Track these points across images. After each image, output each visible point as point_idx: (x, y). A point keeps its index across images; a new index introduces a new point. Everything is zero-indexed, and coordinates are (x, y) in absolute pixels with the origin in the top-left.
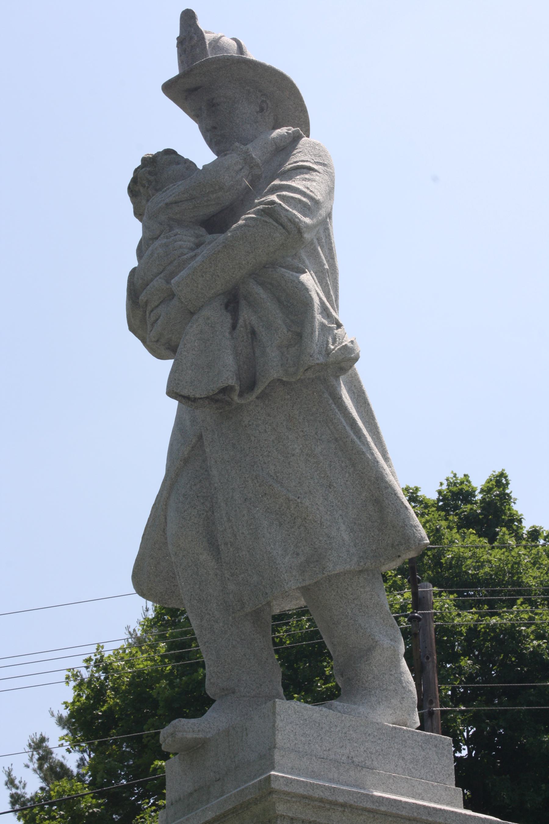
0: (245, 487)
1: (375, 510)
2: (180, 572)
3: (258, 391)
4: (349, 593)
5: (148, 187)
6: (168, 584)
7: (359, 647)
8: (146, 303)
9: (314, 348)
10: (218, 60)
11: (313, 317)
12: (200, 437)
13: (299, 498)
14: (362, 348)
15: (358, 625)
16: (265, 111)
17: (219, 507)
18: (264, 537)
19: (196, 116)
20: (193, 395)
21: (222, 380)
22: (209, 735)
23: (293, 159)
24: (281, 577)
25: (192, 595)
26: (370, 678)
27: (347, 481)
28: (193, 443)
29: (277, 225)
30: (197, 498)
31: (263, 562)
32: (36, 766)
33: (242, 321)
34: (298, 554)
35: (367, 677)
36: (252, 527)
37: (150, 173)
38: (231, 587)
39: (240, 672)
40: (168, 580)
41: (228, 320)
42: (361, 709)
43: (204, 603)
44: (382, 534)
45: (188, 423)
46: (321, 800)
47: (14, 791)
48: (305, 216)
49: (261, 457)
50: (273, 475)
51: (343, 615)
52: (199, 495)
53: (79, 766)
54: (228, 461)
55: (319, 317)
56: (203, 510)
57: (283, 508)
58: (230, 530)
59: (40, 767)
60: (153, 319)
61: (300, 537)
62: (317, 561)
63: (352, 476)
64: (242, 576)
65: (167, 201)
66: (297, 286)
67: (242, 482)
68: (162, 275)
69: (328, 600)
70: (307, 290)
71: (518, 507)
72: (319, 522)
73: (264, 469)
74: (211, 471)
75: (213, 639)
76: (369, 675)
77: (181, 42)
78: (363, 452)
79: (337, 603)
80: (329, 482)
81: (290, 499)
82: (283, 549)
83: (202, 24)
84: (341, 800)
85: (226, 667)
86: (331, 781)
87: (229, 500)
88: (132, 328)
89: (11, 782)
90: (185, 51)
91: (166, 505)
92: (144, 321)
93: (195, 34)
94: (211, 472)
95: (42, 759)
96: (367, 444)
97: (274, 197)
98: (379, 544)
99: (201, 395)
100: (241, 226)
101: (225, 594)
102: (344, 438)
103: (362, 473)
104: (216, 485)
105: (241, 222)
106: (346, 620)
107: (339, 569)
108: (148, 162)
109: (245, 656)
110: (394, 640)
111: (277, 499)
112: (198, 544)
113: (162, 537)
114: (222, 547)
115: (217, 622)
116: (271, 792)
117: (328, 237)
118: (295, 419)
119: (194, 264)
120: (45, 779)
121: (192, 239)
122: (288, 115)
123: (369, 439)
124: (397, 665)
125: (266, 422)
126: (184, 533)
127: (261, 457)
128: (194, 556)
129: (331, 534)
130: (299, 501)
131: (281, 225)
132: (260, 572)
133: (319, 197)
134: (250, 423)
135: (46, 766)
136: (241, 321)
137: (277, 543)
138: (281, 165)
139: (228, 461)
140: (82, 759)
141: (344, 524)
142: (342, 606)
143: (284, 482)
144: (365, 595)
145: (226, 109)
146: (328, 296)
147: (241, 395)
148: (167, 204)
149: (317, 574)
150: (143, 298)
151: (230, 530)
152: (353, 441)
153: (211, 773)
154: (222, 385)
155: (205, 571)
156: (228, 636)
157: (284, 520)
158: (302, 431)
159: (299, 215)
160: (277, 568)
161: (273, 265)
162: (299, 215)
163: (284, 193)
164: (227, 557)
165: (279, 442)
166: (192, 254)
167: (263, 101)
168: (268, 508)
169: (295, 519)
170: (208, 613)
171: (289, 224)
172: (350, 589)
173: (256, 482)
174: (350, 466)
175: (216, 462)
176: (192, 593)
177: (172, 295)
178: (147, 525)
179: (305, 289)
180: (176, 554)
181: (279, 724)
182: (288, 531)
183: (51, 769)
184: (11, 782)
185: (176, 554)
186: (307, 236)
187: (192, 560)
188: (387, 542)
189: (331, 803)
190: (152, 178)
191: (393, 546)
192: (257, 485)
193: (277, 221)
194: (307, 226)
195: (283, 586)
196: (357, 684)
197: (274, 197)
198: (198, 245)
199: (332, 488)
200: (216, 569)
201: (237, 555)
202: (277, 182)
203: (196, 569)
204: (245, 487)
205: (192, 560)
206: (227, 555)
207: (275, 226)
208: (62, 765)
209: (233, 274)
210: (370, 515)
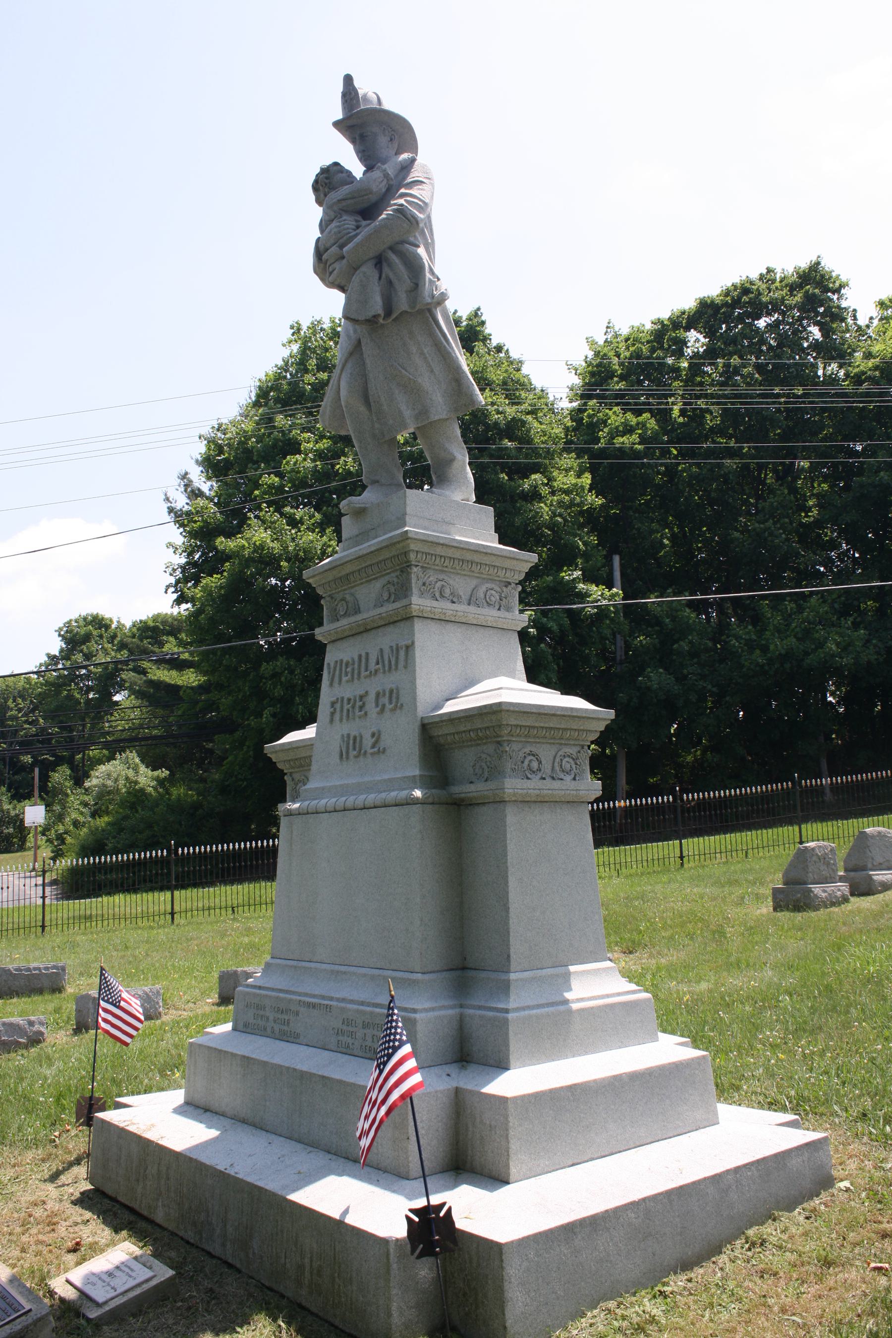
3: (394, 316)
9: (426, 293)
10: (367, 109)
11: (425, 275)
12: (359, 342)
14: (450, 293)
19: (353, 141)
23: (412, 175)
32: (183, 490)
38: (377, 426)
42: (447, 493)
45: (352, 332)
46: (432, 542)
47: (169, 505)
48: (420, 213)
53: (210, 490)
55: (428, 275)
59: (186, 491)
60: (331, 269)
70: (422, 259)
71: (488, 329)
77: (344, 95)
83: (356, 84)
84: (441, 542)
86: (434, 531)
88: (315, 272)
89: (167, 499)
90: (346, 101)
92: (324, 270)
95: (186, 486)
96: (452, 348)
97: (401, 201)
100: (384, 219)
105: (383, 216)
107: (437, 418)
110: (464, 456)
114: (372, 404)
116: (408, 539)
117: (431, 226)
119: (357, 240)
120: (189, 498)
121: (354, 223)
123: (453, 345)
124: (465, 469)
133: (427, 201)
135: (189, 489)
136: (384, 276)
138: (404, 178)
140: (212, 486)
146: (430, 259)
147: (384, 319)
150: (325, 257)
152: (445, 346)
159: (417, 213)
161: (403, 242)
162: (417, 213)
163: (409, 199)
166: (354, 233)
177: (343, 257)
179: (419, 258)
181: (408, 502)
183: (193, 491)
184: (167, 499)
186: (421, 225)
189: (437, 543)
190: (327, 181)
193: (404, 216)
194: (422, 220)
197: (401, 201)
198: (358, 227)
202: (403, 190)
208: (199, 489)
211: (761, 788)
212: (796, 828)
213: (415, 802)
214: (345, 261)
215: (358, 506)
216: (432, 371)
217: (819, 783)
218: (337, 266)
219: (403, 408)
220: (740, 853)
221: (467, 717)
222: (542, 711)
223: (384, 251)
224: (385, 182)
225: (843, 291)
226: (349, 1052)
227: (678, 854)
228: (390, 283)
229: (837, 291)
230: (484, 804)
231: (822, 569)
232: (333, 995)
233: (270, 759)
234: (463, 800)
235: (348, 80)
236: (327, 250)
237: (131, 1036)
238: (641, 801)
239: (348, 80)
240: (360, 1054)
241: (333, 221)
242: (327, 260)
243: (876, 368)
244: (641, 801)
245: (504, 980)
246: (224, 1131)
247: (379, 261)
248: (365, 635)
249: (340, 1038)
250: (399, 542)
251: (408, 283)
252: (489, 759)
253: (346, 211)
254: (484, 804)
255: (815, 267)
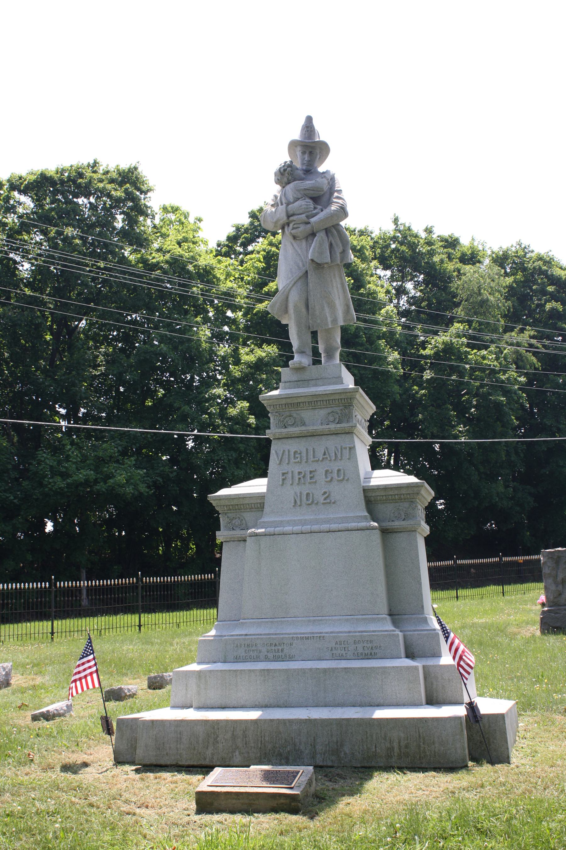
211: (68, 584)
212: (50, 623)
213: (374, 528)
214: (309, 226)
217: (78, 584)
219: (328, 315)
220: (95, 632)
221: (397, 488)
222: (245, 496)
223: (330, 227)
225: (149, 194)
226: (343, 658)
227: (50, 630)
229: (146, 193)
230: (401, 532)
232: (321, 631)
233: (211, 504)
234: (387, 529)
235: (309, 119)
237: (88, 688)
238: (41, 585)
239: (309, 119)
240: (354, 658)
243: (167, 262)
244: (37, 585)
245: (422, 618)
246: (262, 711)
247: (327, 231)
248: (309, 438)
249: (334, 652)
250: (350, 392)
251: (341, 249)
252: (404, 509)
253: (306, 196)
254: (401, 532)
255: (133, 170)
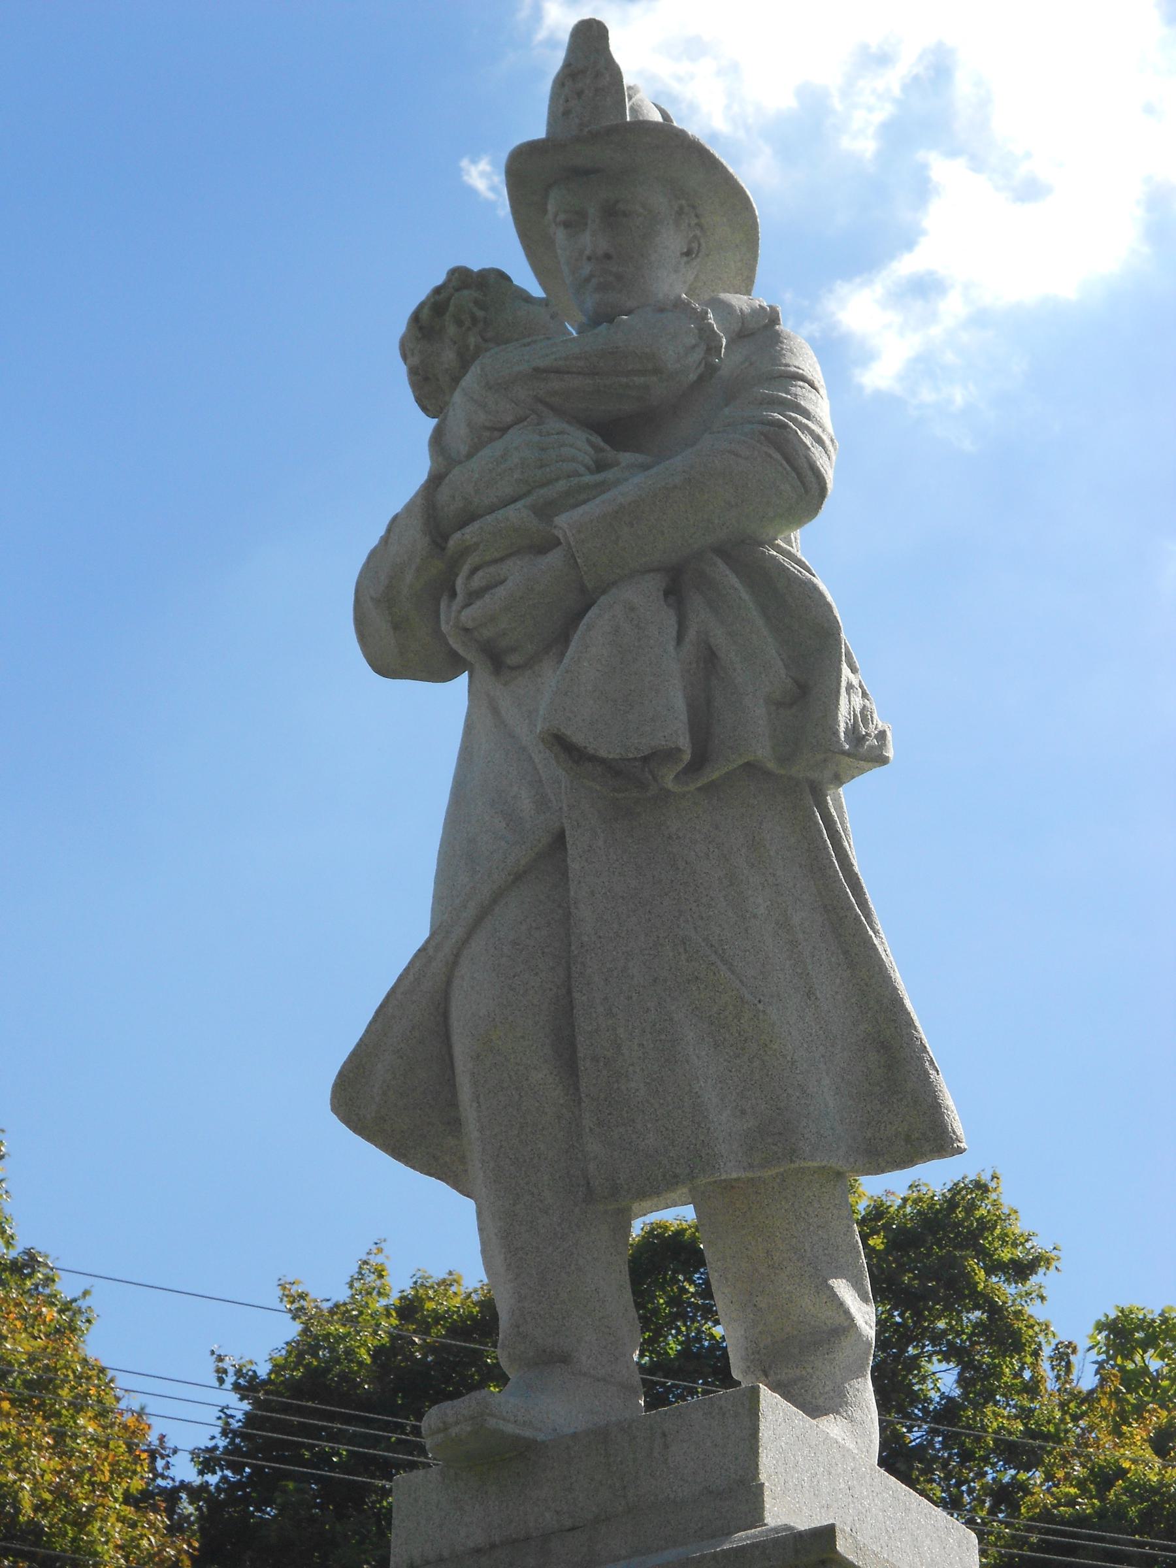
0: (655, 956)
1: (879, 1061)
2: (482, 1096)
3: (714, 773)
4: (813, 1212)
5: (469, 329)
6: (420, 1116)
7: (812, 1323)
8: (465, 552)
11: (839, 671)
12: (559, 840)
13: (760, 1002)
15: (820, 1279)
16: (694, 256)
17: (589, 984)
18: (687, 1061)
20: (595, 749)
21: (666, 734)
22: (541, 1437)
24: (716, 1149)
25: (501, 1147)
26: (827, 1388)
27: (837, 993)
28: (540, 845)
29: (788, 468)
30: (541, 956)
31: (680, 1111)
33: (695, 633)
34: (743, 1112)
35: (824, 1387)
36: (663, 1037)
37: (476, 302)
39: (583, 1324)
40: (421, 1109)
41: (669, 619)
43: (523, 1169)
44: (889, 1111)
49: (695, 904)
50: (717, 945)
51: (795, 1253)
52: (546, 950)
54: (622, 897)
56: (552, 982)
57: (727, 1013)
58: (608, 1034)
60: (477, 582)
61: (751, 1080)
62: (780, 1134)
63: (846, 986)
64: (621, 1130)
65: (541, 364)
66: (810, 595)
67: (651, 945)
68: (528, 501)
69: (771, 1218)
72: (789, 1058)
73: (699, 929)
74: (577, 908)
75: (534, 1244)
76: (827, 1383)
78: (724, 964)
79: (787, 1226)
80: (808, 986)
81: (745, 1001)
82: (718, 1095)
85: (555, 1306)
87: (615, 973)
91: (456, 956)
93: (606, 69)
94: (576, 911)
98: (879, 1129)
99: (609, 753)
101: (571, 1159)
102: (842, 908)
103: (867, 985)
104: (585, 939)
106: (800, 1264)
108: (461, 278)
109: (598, 1293)
111: (718, 994)
112: (534, 1048)
113: (432, 1017)
115: (546, 1213)
118: (763, 848)
122: (720, 278)
125: (710, 839)
126: (511, 1018)
127: (695, 904)
128: (518, 1070)
129: (808, 1088)
130: (760, 1007)
131: (795, 469)
132: (667, 1129)
134: (681, 834)
136: (691, 635)
137: (710, 1080)
139: (622, 897)
141: (827, 1074)
142: (796, 1235)
143: (736, 964)
144: (838, 1223)
145: (638, 227)
148: (536, 370)
149: (779, 1158)
151: (608, 1034)
152: (857, 917)
153: (547, 1515)
154: (664, 743)
155: (537, 1104)
156: (570, 1246)
157: (724, 1039)
158: (774, 875)
160: (709, 1129)
164: (594, 1085)
165: (732, 884)
167: (695, 237)
168: (696, 1008)
169: (746, 1040)
170: (530, 1191)
171: (809, 473)
172: (816, 1205)
173: (681, 950)
174: (845, 967)
175: (593, 893)
176: (503, 1143)
178: (393, 990)
180: (478, 1056)
182: (729, 1062)
185: (478, 1056)
187: (510, 1077)
188: (896, 1129)
190: (480, 314)
191: (908, 1139)
192: (683, 957)
195: (717, 1166)
196: (801, 1395)
198: (600, 466)
199: (813, 999)
200: (562, 1105)
201: (616, 1086)
203: (517, 1097)
204: (655, 956)
205: (510, 1077)
206: (594, 1082)
207: (785, 469)
209: (691, 537)
210: (868, 1068)
214: (554, 558)
215: (510, 1428)
216: (810, 994)
218: (516, 572)
224: (698, 355)
228: (709, 658)
231: (287, 1454)
236: (468, 517)
241: (504, 430)
242: (465, 552)
